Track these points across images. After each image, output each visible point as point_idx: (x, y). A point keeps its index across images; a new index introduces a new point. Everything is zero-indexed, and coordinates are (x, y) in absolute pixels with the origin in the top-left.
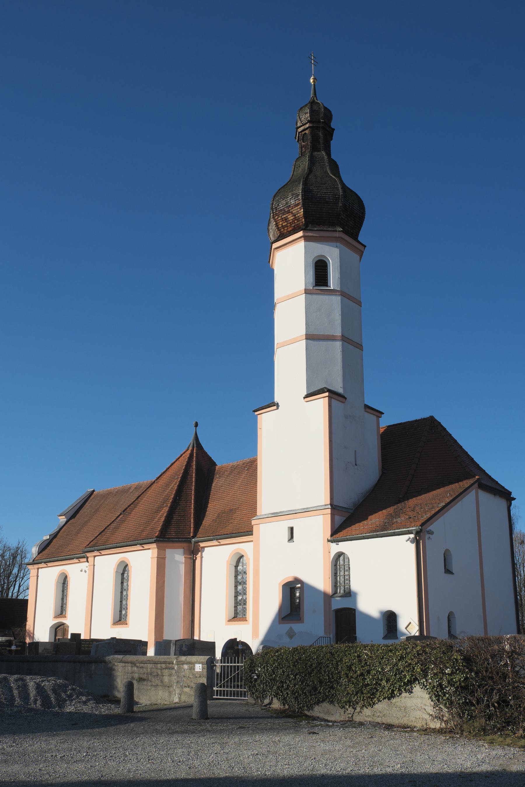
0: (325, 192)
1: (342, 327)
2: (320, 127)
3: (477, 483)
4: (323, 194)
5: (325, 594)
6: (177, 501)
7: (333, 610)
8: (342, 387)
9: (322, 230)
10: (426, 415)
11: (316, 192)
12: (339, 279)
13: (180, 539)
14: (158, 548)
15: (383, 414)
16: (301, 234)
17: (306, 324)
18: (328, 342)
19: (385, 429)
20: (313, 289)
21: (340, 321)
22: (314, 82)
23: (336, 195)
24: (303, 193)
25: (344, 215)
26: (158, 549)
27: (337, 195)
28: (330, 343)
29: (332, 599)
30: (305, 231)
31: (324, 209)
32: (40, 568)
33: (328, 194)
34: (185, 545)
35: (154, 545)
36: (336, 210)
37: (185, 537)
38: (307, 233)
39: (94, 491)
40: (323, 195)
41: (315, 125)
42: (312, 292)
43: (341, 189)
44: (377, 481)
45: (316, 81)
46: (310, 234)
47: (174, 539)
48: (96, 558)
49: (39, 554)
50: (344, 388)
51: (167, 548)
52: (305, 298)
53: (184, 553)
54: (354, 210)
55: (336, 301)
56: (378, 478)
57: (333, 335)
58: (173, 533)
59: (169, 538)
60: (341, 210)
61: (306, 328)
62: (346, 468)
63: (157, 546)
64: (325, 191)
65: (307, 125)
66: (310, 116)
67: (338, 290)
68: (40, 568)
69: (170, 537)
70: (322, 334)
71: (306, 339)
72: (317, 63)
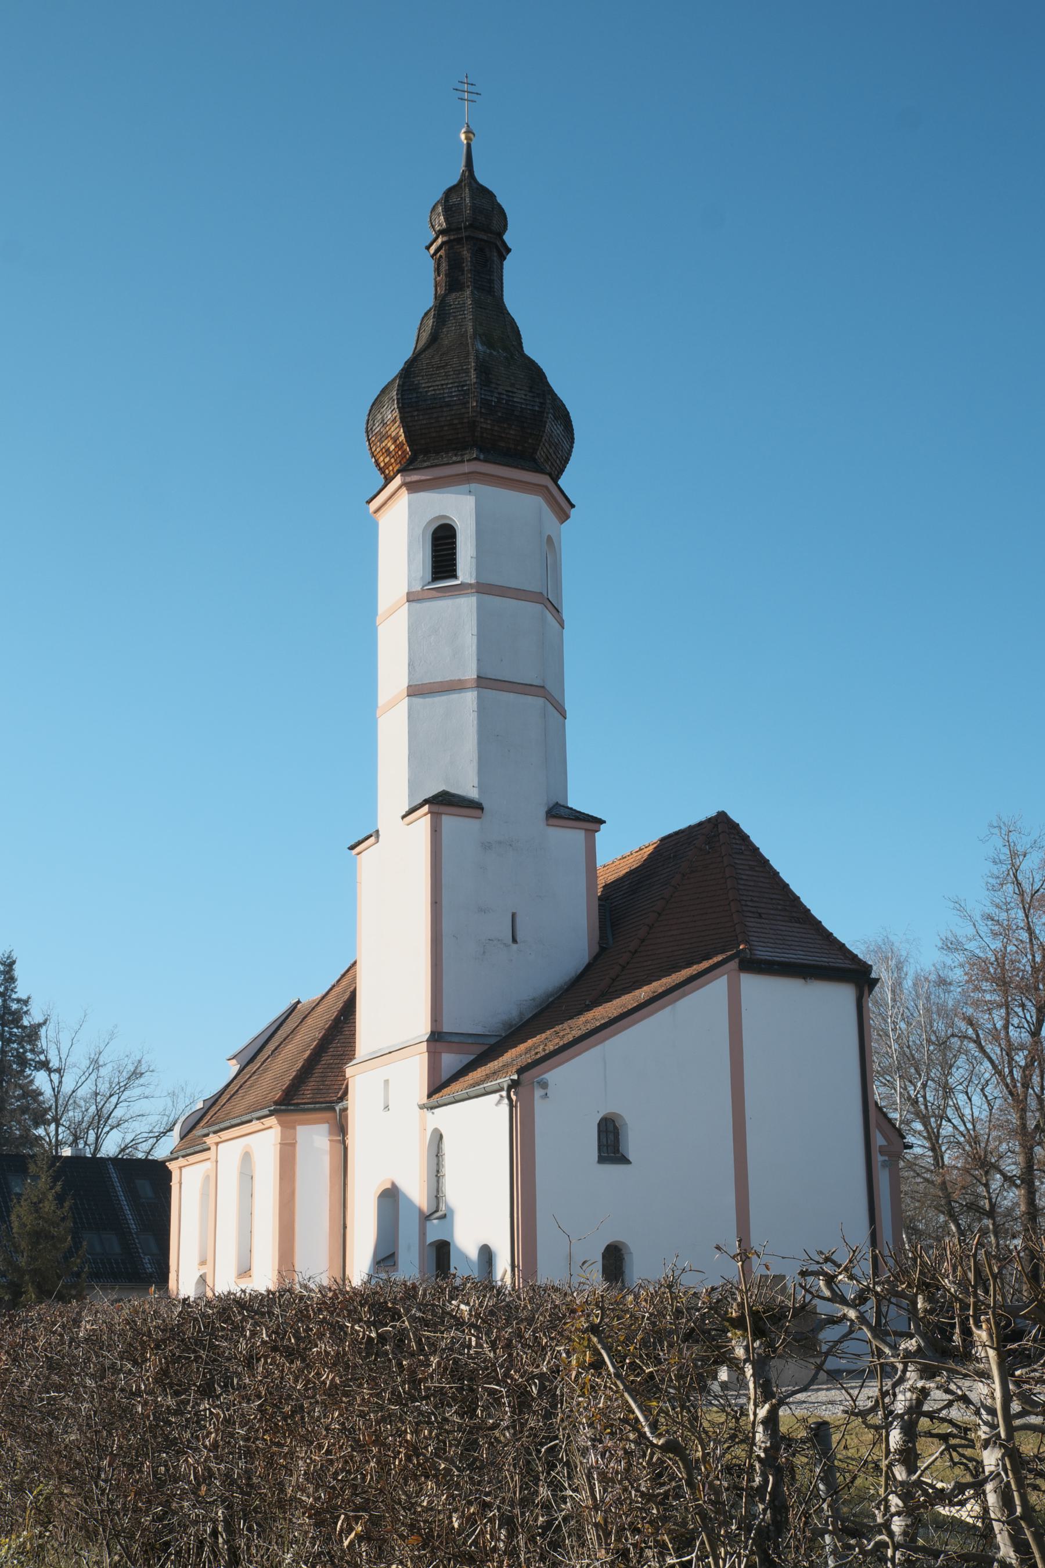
0: (442, 385)
1: (478, 660)
2: (462, 238)
3: (737, 960)
4: (439, 389)
5: (421, 1211)
6: (340, 1026)
7: (431, 1244)
8: (476, 785)
9: (436, 466)
10: (712, 813)
11: (425, 388)
12: (474, 560)
13: (317, 1106)
14: (281, 1123)
15: (604, 822)
16: (398, 480)
17: (409, 665)
18: (427, 699)
19: (655, 845)
20: (422, 590)
21: (474, 648)
22: (467, 138)
23: (463, 386)
24: (399, 396)
25: (489, 422)
26: (281, 1126)
27: (466, 385)
28: (455, 697)
29: (428, 1223)
30: (405, 474)
31: (444, 419)
32: (184, 1166)
33: (449, 386)
34: (328, 1115)
35: (272, 1121)
36: (466, 415)
37: (327, 1099)
38: (409, 476)
39: (299, 1002)
40: (438, 392)
41: (452, 237)
42: (420, 598)
43: (475, 370)
44: (582, 968)
45: (471, 136)
46: (415, 477)
47: (306, 1106)
48: (220, 1146)
49: (182, 1139)
50: (481, 786)
51: (299, 1124)
52: (409, 610)
53: (331, 1133)
54: (516, 404)
55: (467, 606)
56: (586, 960)
57: (460, 680)
58: (309, 1092)
59: (298, 1104)
60: (474, 414)
61: (410, 673)
62: (484, 952)
63: (278, 1120)
64: (443, 382)
65: (440, 241)
66: (446, 220)
67: (471, 584)
68: (184, 1166)
69: (299, 1101)
70: (439, 680)
71: (483, 682)
72: (477, 94)
